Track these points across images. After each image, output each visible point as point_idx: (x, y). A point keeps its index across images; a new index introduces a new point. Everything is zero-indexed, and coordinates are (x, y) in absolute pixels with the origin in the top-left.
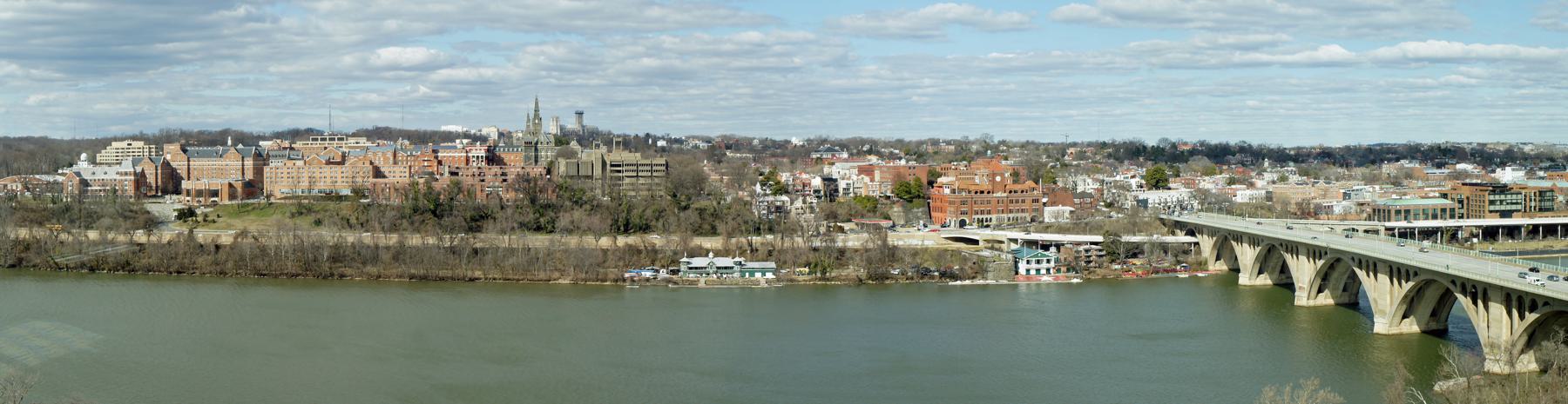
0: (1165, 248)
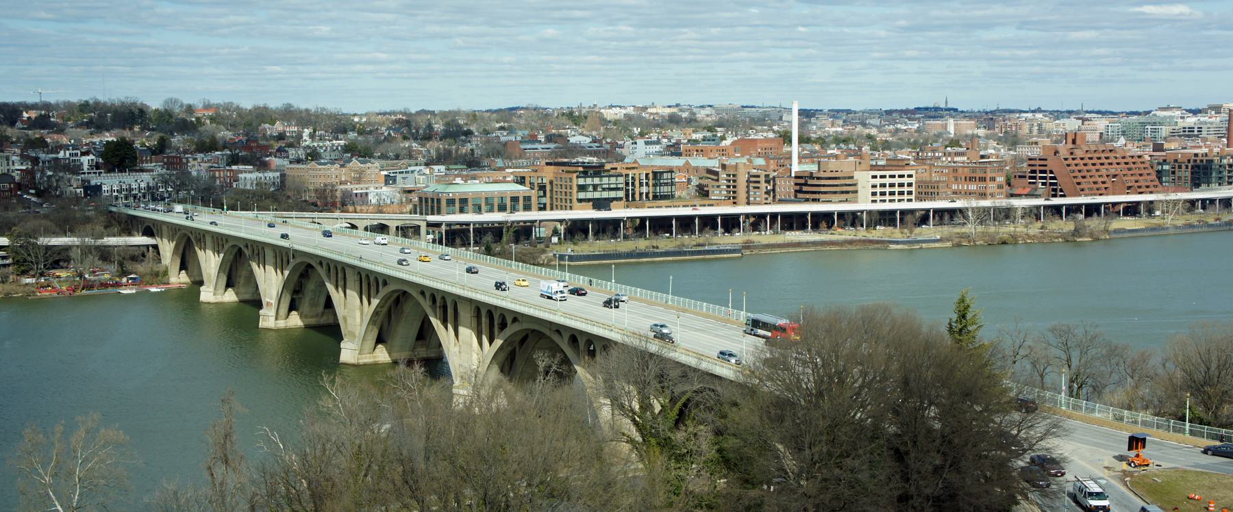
0: (105, 254)
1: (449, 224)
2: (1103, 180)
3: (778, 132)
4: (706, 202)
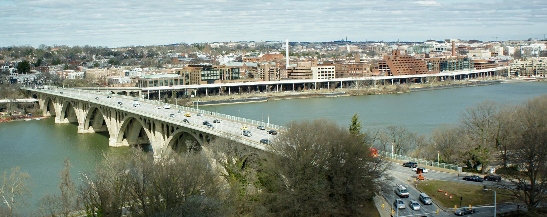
0: (19, 105)
1: (150, 91)
2: (407, 69)
3: (281, 52)
4: (253, 80)
